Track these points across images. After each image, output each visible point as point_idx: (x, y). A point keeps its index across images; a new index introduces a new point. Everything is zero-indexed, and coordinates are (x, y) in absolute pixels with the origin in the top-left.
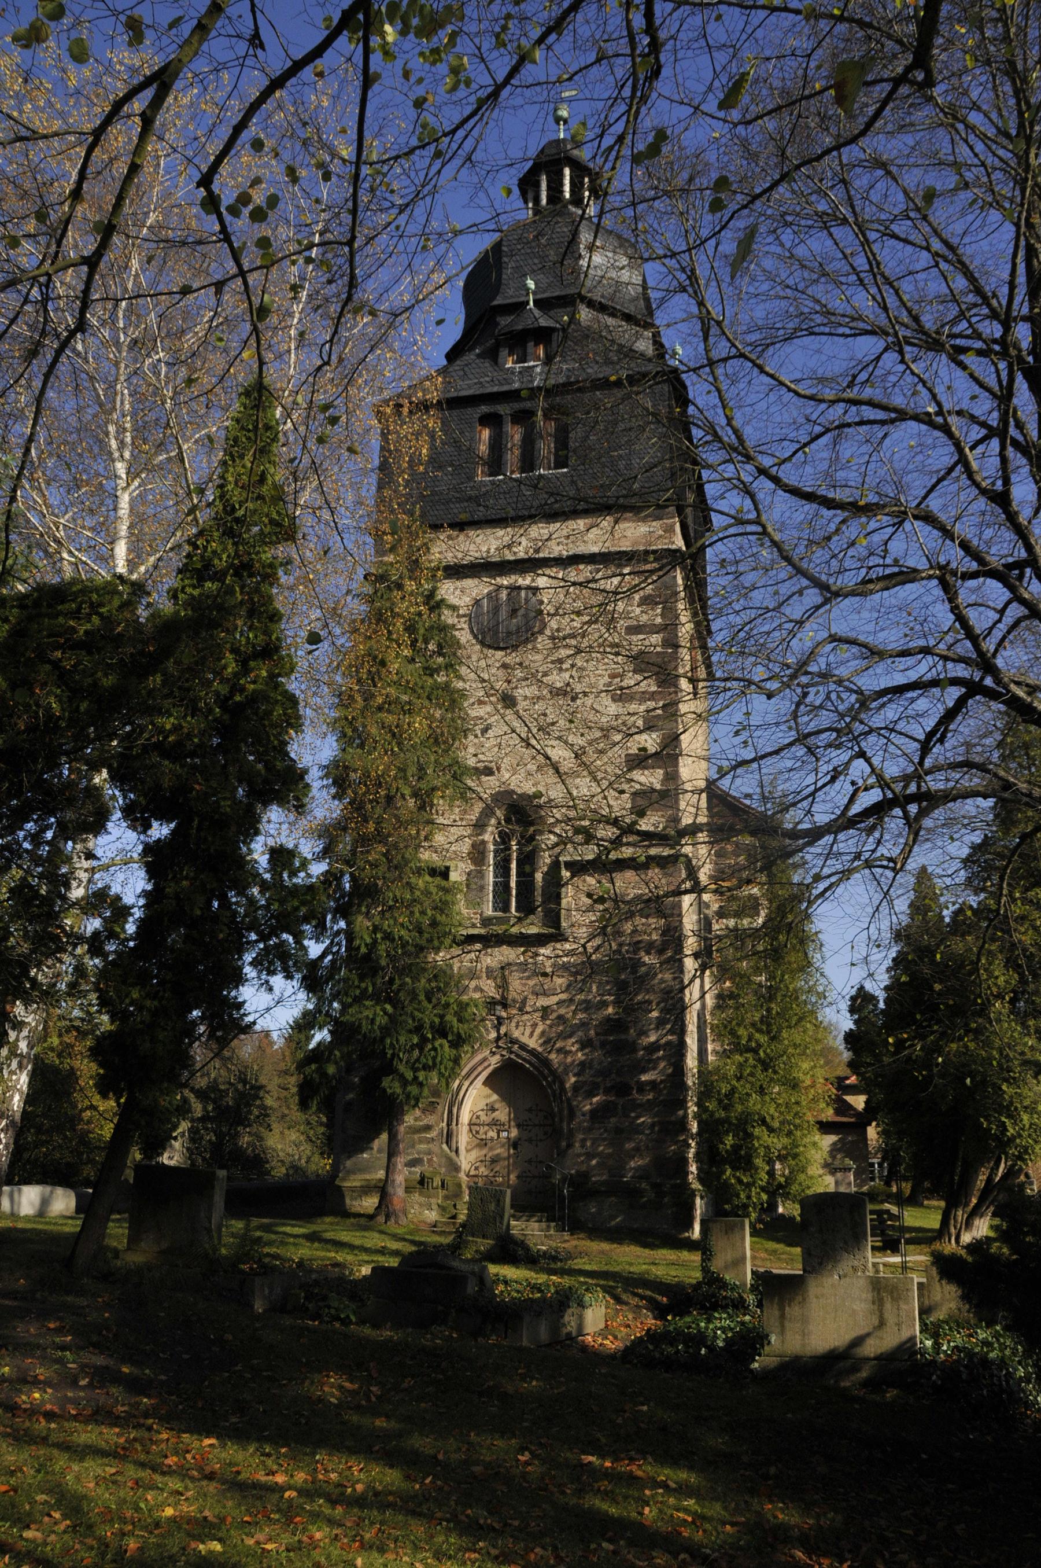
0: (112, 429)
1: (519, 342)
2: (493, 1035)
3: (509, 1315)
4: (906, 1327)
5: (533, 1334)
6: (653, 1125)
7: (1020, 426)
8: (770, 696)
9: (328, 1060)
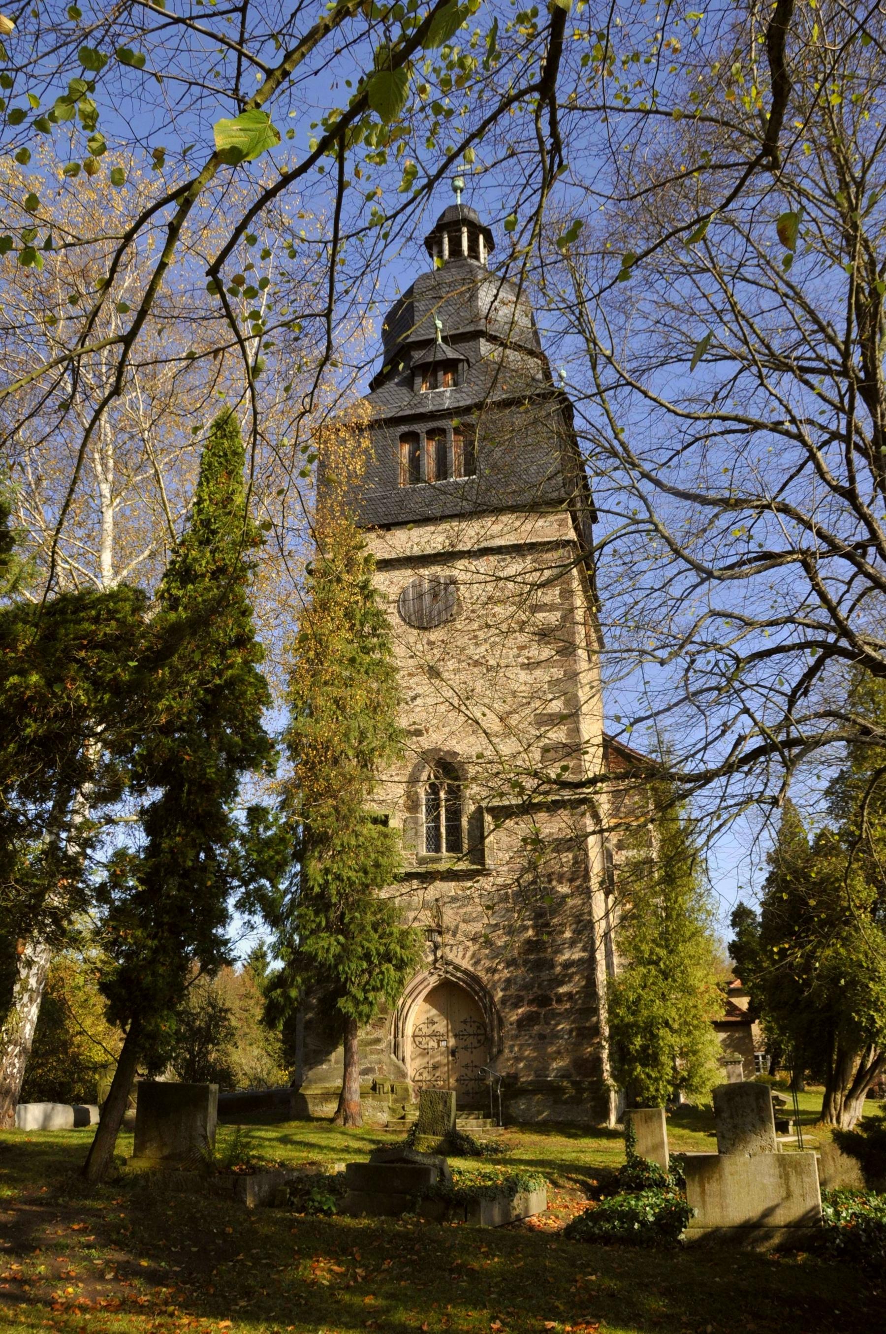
0: (97, 456)
1: (431, 371)
2: (431, 958)
3: (467, 1202)
4: (807, 1199)
5: (490, 1216)
6: (571, 1031)
7: (859, 433)
8: (662, 663)
9: (292, 985)
